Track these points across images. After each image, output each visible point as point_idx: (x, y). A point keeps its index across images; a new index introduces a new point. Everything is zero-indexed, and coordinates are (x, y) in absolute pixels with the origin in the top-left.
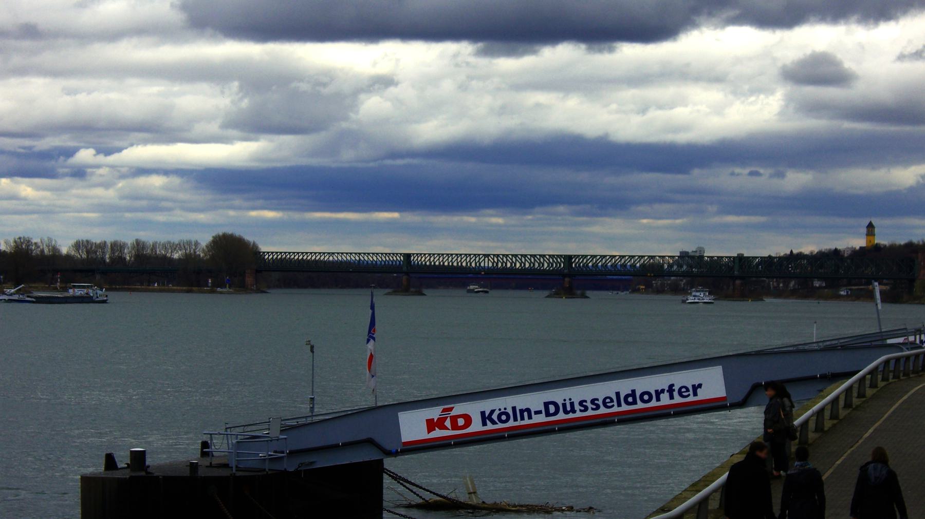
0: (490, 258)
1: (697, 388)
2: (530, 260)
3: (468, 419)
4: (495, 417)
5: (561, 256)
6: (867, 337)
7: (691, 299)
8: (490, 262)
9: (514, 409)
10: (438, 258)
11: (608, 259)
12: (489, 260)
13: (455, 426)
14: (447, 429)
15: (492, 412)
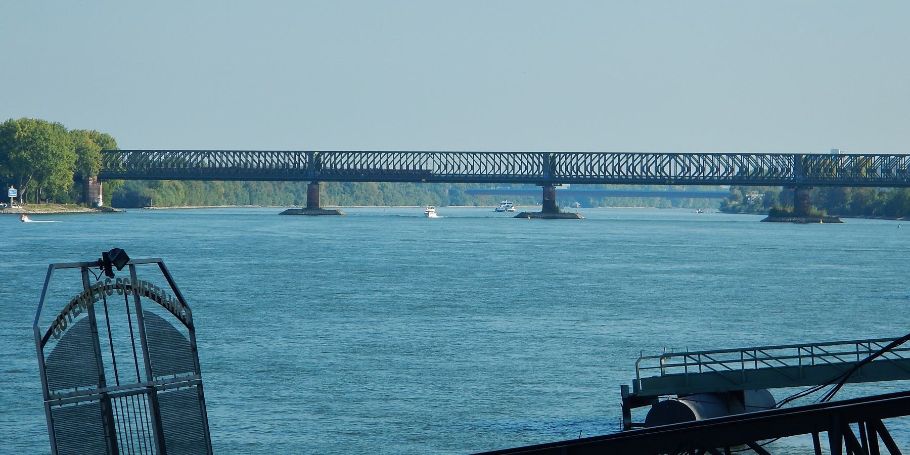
0: (678, 159)
1: (83, 297)
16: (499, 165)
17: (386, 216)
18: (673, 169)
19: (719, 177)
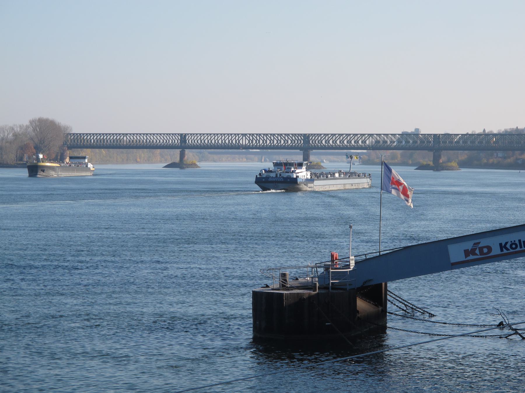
0: (247, 137)
3: (490, 249)
4: (508, 246)
5: (301, 134)
6: (152, 174)
7: (279, 161)
8: (246, 139)
9: (520, 241)
10: (214, 137)
11: (352, 137)
12: (246, 138)
13: (481, 253)
14: (477, 255)
15: (506, 243)
16: (246, 139)
18: (244, 142)
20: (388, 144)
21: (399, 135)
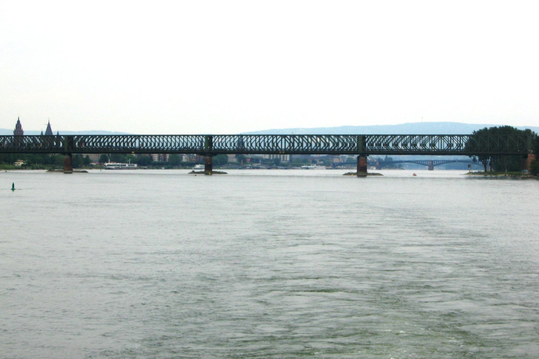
0: (286, 138)
2: (299, 140)
8: (286, 142)
12: (285, 140)
17: (232, 175)
19: (320, 149)
20: (321, 147)
21: (467, 135)
